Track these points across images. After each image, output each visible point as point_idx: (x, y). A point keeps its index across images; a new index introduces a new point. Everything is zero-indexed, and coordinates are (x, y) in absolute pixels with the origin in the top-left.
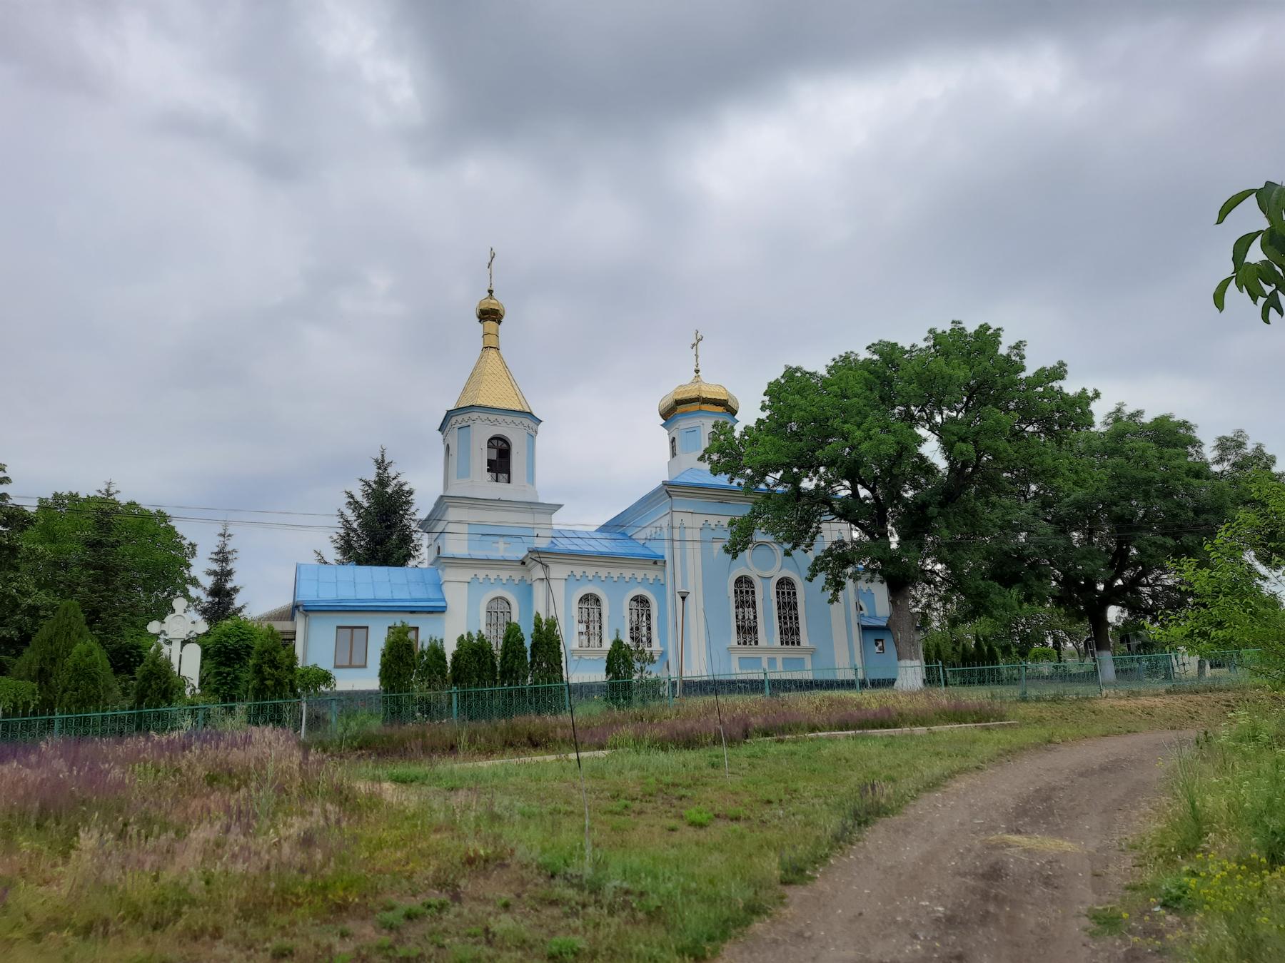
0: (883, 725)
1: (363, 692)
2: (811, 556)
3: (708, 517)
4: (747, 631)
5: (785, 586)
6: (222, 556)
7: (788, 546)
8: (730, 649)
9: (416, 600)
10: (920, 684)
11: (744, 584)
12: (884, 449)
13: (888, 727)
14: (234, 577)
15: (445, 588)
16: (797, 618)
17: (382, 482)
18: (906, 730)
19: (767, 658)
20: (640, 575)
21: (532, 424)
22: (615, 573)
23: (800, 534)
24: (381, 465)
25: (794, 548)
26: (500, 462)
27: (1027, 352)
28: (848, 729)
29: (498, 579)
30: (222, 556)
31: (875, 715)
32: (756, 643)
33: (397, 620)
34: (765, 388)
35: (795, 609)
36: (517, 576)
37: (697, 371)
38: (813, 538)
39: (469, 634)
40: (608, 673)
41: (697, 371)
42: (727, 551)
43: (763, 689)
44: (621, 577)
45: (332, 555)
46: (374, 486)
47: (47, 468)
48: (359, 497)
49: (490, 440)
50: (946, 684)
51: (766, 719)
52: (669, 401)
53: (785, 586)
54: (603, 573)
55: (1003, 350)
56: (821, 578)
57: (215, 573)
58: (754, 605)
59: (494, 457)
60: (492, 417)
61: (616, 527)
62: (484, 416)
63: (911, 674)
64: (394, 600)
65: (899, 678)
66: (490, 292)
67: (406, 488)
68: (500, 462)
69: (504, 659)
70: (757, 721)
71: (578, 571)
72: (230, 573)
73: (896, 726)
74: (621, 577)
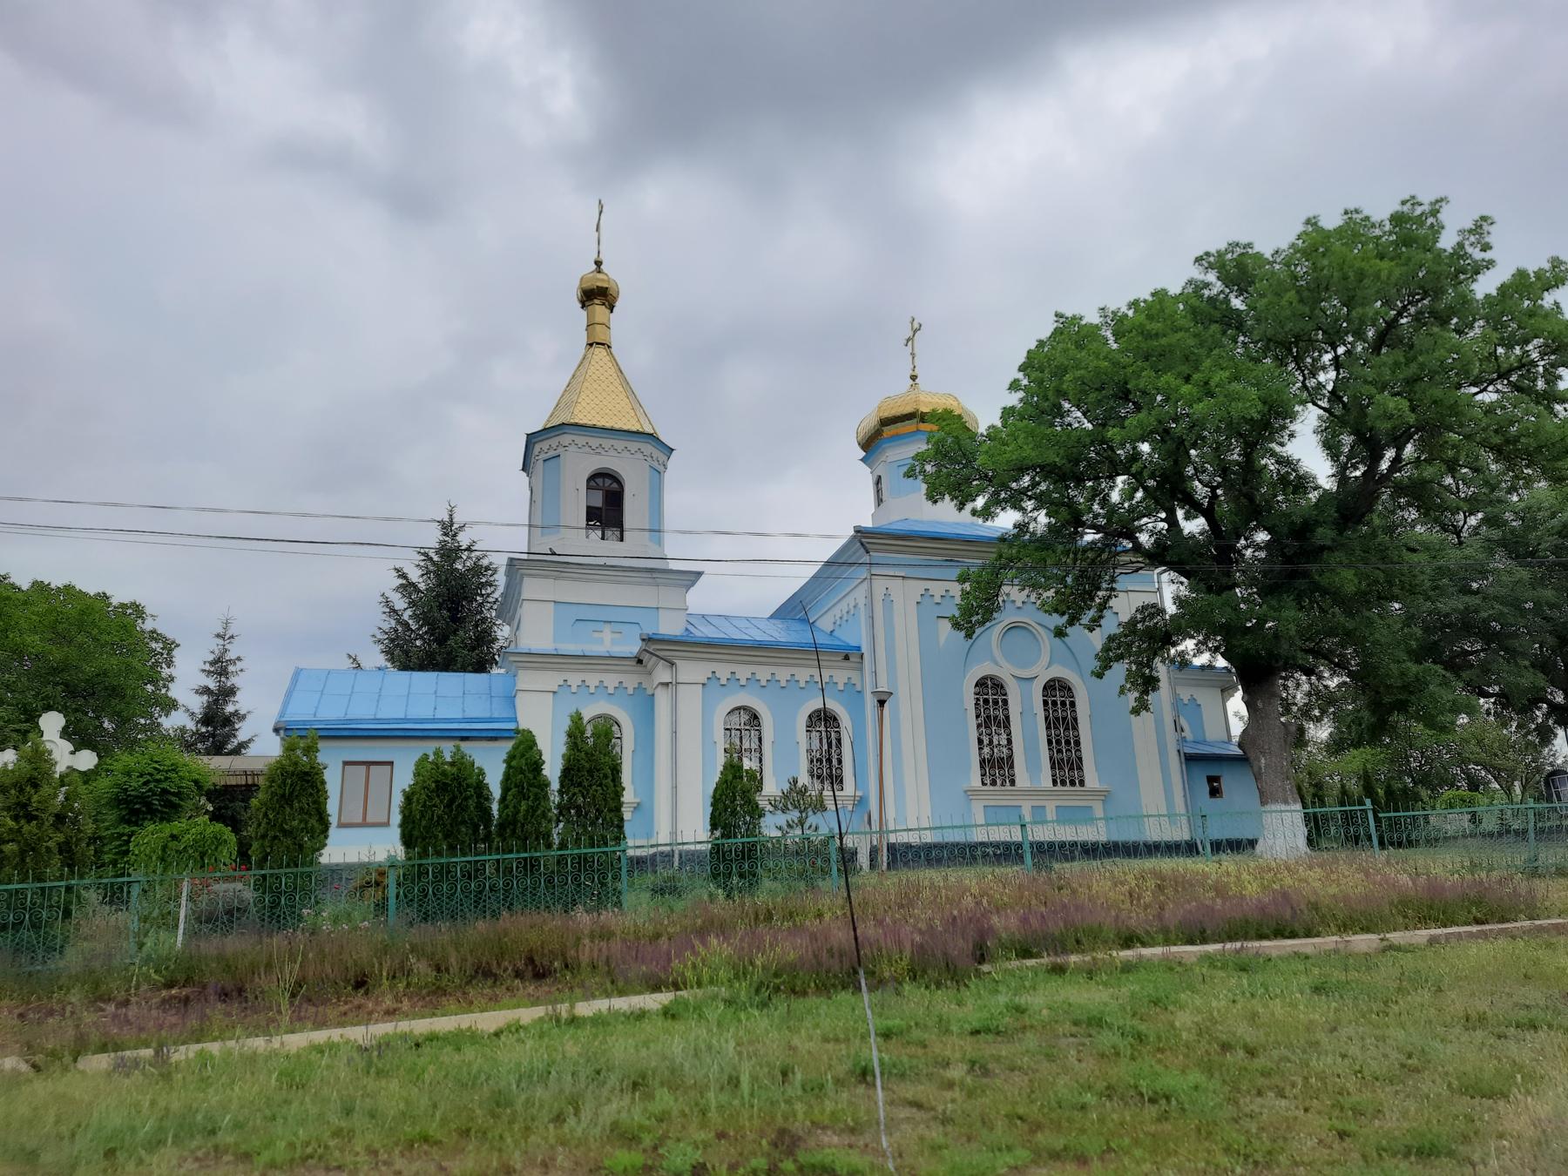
0: (1281, 931)
2: (1097, 639)
3: (928, 584)
4: (997, 767)
5: (1057, 694)
6: (220, 667)
7: (1061, 621)
8: (970, 793)
10: (1301, 842)
11: (990, 692)
12: (1237, 409)
13: (1293, 935)
14: (239, 696)
16: (1077, 743)
17: (449, 552)
18: (1329, 941)
19: (1036, 808)
21: (657, 453)
22: (783, 674)
23: (1079, 598)
24: (448, 528)
25: (1071, 623)
26: (607, 508)
27: (1495, 236)
28: (1204, 941)
29: (601, 686)
30: (220, 667)
31: (1262, 909)
32: (1013, 783)
33: (429, 748)
34: (1022, 359)
35: (1075, 728)
36: (631, 682)
37: (914, 378)
38: (1103, 606)
40: (714, 826)
41: (914, 378)
42: (957, 626)
43: (1021, 858)
44: (792, 680)
45: (375, 657)
46: (436, 558)
47: (30, 564)
48: (415, 575)
49: (589, 480)
50: (1382, 844)
51: (1024, 920)
52: (871, 422)
53: (1057, 694)
54: (763, 673)
55: (1447, 242)
56: (1119, 670)
57: (206, 691)
58: (1006, 723)
60: (594, 442)
61: (795, 609)
62: (581, 440)
63: (1283, 830)
65: (1261, 842)
66: (598, 263)
67: (485, 562)
68: (607, 508)
69: (503, 799)
70: (1005, 924)
71: (723, 671)
72: (230, 692)
73: (1308, 934)
74: (792, 680)
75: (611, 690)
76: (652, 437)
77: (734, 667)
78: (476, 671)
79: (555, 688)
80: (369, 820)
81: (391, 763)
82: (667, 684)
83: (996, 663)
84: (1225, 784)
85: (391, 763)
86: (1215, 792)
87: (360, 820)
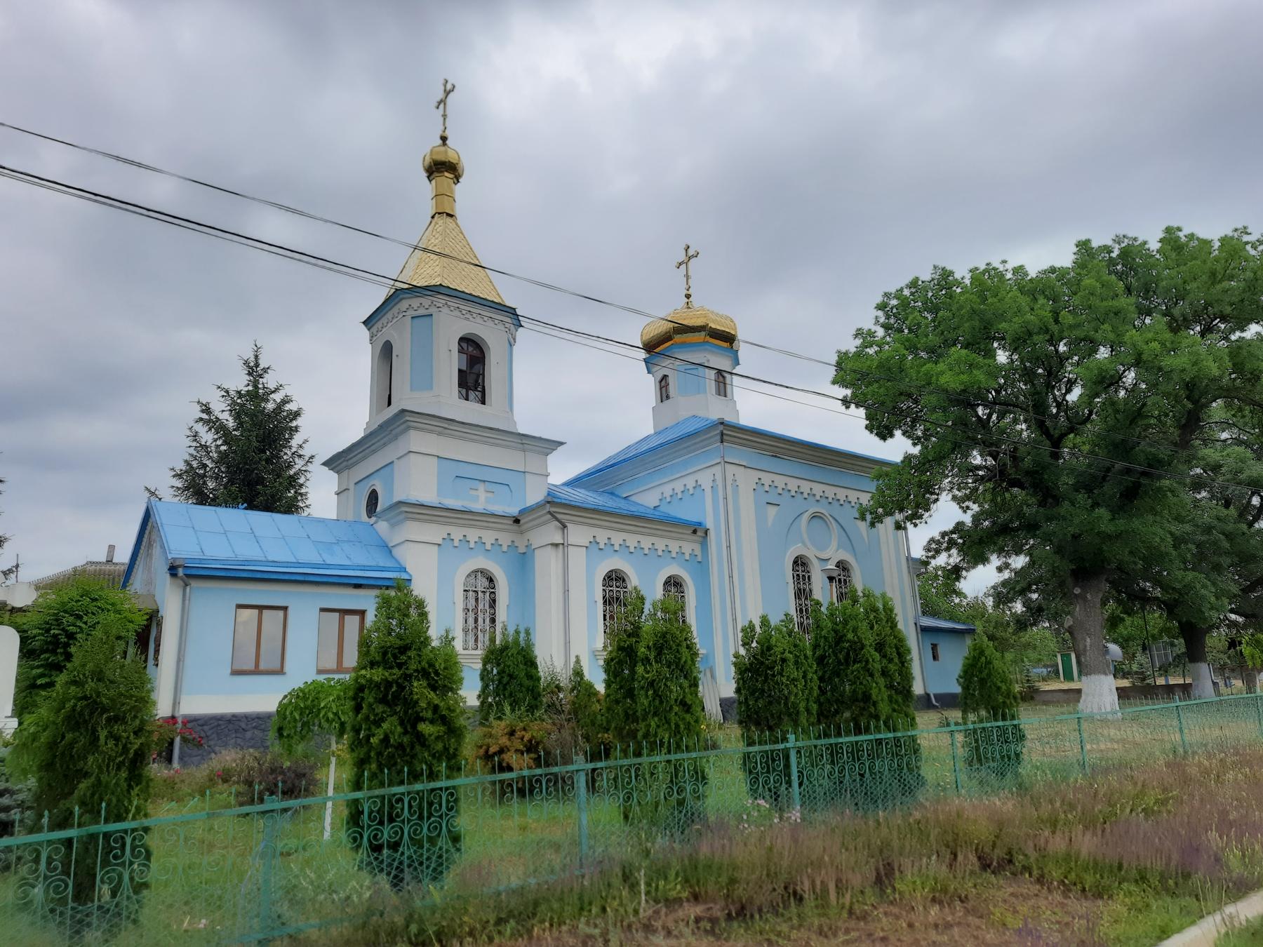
1: (247, 718)
3: (761, 474)
9: (364, 568)
15: (395, 552)
17: (256, 395)
20: (674, 546)
24: (254, 370)
29: (480, 542)
36: (505, 539)
37: (688, 296)
39: (765, 622)
41: (688, 296)
54: (632, 541)
59: (464, 368)
64: (329, 566)
66: (444, 139)
67: (292, 407)
71: (602, 535)
75: (488, 547)
76: (512, 312)
77: (654, 540)
78: (286, 512)
79: (440, 542)
80: (262, 666)
81: (285, 609)
82: (557, 545)
84: (940, 650)
85: (285, 609)
86: (935, 657)
87: (251, 666)
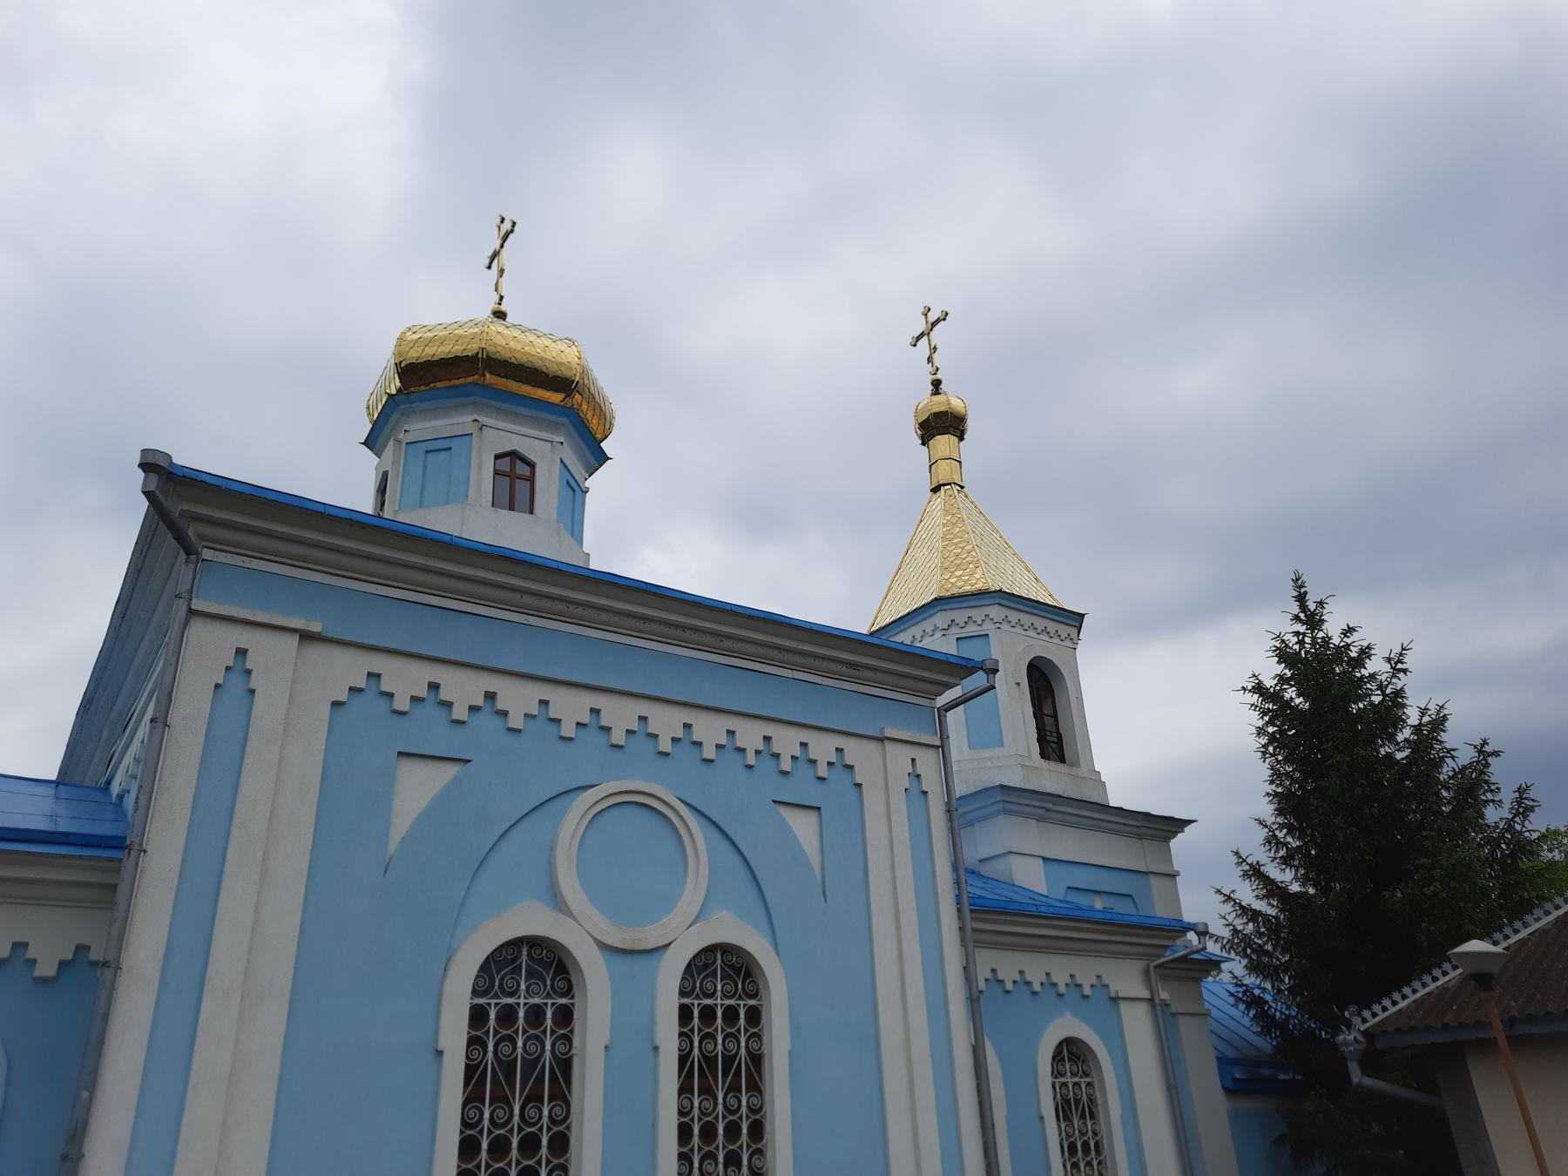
83: (558, 903)
